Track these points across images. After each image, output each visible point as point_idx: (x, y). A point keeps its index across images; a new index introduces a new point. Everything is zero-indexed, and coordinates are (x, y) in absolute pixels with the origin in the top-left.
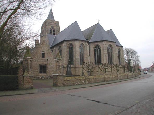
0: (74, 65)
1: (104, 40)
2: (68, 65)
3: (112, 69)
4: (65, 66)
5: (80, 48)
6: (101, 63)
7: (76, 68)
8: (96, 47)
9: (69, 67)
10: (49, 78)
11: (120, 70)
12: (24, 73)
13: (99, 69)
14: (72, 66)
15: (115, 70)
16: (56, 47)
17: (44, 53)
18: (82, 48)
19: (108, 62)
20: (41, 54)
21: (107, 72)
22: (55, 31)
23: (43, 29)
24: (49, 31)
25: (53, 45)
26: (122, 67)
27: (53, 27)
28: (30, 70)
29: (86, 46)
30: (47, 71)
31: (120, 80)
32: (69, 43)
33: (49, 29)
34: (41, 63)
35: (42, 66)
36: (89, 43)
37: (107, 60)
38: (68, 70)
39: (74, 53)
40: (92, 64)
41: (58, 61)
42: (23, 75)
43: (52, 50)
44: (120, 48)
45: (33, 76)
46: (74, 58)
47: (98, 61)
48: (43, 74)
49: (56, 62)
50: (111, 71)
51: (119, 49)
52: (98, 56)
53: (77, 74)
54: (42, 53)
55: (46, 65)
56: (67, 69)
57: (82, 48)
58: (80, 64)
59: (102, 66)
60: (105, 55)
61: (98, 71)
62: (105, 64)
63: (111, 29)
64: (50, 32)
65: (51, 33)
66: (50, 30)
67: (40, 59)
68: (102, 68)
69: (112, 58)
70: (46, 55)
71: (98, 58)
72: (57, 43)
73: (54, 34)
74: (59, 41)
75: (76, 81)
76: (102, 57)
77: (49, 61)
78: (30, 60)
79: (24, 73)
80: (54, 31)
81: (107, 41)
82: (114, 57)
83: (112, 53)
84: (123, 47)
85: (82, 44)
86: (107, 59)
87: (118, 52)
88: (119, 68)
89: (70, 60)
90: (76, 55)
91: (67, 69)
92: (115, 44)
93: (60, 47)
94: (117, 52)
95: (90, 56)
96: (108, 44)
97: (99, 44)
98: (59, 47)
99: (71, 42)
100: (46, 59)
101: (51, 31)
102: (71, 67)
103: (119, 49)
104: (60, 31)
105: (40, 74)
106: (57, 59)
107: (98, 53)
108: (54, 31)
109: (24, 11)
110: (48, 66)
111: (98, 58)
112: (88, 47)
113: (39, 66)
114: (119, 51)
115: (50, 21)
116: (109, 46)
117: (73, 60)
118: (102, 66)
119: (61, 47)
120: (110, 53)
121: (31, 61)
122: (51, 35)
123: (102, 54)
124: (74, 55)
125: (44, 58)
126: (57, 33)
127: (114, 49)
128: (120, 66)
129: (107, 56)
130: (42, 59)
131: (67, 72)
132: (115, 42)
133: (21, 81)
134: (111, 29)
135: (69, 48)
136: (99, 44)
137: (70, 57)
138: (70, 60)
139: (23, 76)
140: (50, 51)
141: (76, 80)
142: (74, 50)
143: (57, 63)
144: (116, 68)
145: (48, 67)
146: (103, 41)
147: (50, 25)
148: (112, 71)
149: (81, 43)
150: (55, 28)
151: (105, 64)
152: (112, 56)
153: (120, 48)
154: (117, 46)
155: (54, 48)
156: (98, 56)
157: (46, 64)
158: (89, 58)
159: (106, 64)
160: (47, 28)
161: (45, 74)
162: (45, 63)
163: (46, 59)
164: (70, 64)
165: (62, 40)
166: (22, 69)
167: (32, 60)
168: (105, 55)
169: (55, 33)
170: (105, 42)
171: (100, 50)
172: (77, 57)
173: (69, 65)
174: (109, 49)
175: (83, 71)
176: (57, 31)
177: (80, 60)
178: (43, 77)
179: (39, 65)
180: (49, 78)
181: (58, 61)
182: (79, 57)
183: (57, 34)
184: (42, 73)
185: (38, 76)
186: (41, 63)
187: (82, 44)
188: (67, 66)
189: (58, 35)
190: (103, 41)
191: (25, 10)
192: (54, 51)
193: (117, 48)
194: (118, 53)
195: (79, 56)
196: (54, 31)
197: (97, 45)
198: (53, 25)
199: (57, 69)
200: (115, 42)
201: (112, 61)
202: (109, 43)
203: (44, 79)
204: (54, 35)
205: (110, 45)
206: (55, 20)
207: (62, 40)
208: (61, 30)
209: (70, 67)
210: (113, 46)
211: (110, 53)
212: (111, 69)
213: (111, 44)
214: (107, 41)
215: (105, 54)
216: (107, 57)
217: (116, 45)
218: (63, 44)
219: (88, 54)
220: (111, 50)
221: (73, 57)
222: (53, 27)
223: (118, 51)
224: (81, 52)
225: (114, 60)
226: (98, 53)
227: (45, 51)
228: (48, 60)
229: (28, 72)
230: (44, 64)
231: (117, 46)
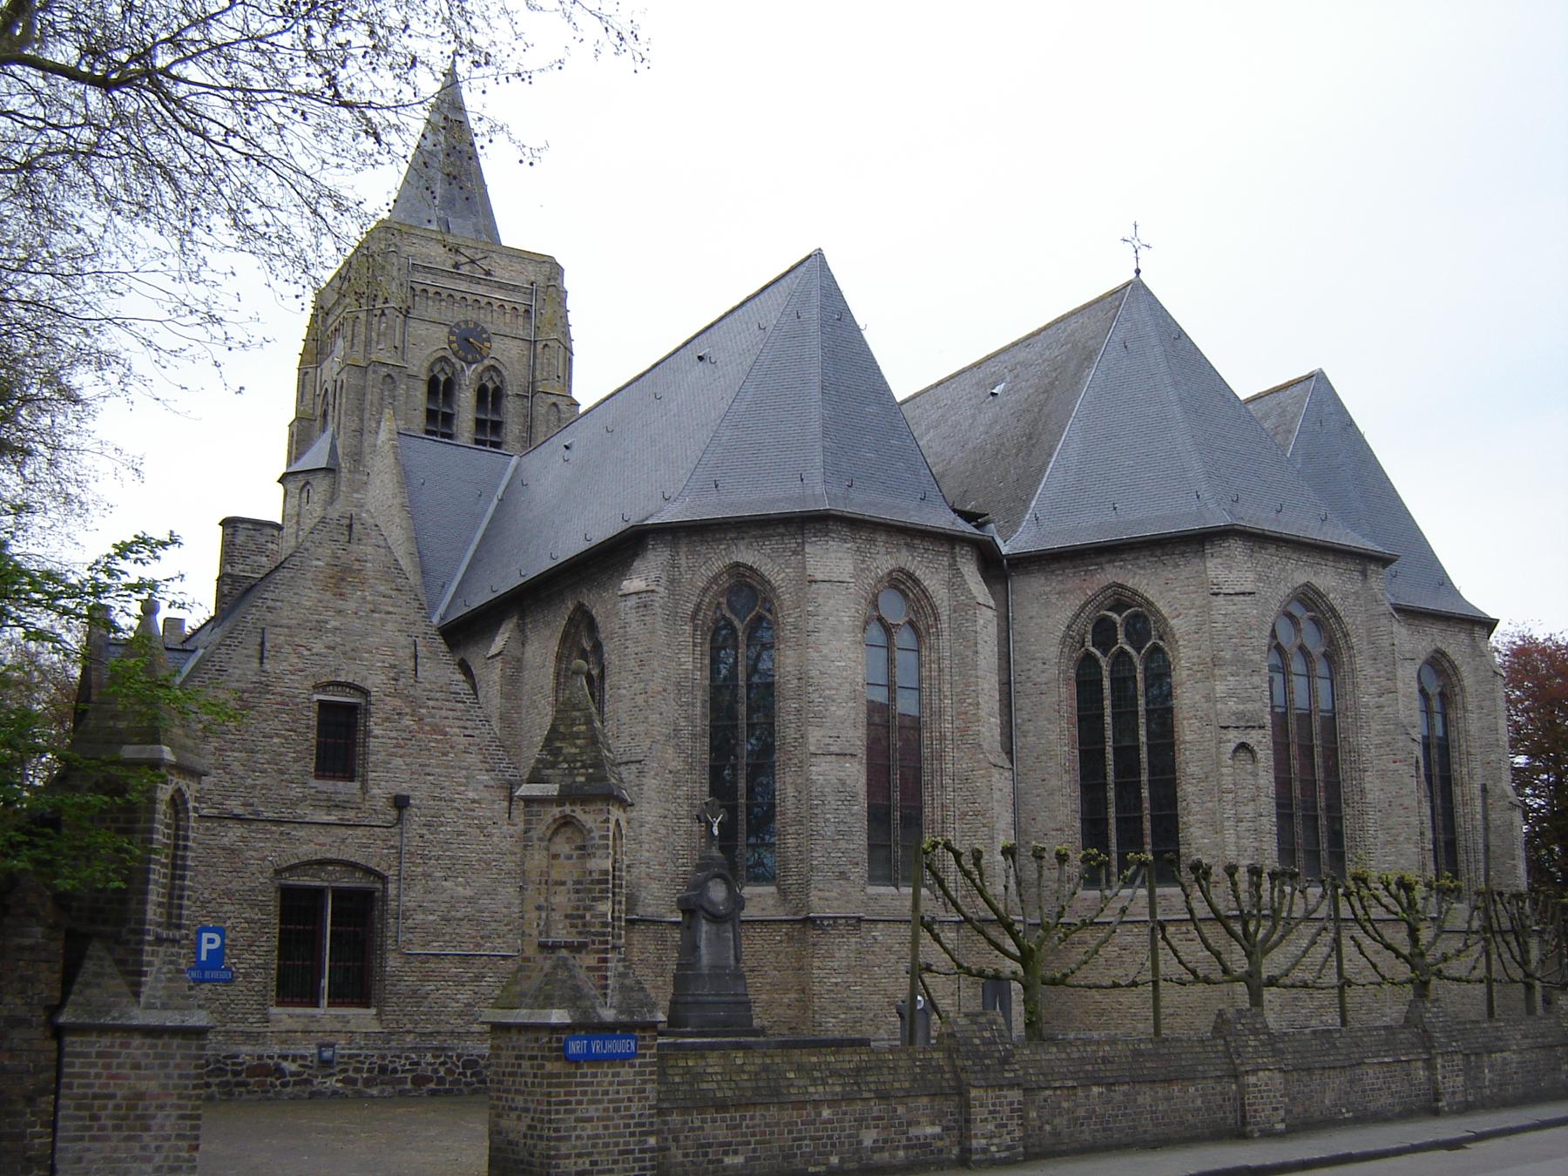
0: (783, 893)
1: (1220, 519)
2: (700, 887)
3: (1348, 948)
4: (658, 900)
5: (875, 632)
6: (1166, 866)
7: (812, 936)
8: (1104, 632)
9: (715, 918)
10: (419, 1081)
11: (1457, 968)
12: (66, 993)
13: (1165, 955)
14: (760, 900)
15: (1385, 960)
16: (521, 628)
17: (352, 708)
18: (904, 638)
19: (1286, 850)
20: (312, 717)
21: (1268, 994)
22: (498, 394)
23: (331, 369)
24: (420, 393)
25: (480, 597)
26: (1487, 928)
27: (469, 342)
28: (159, 941)
29: (964, 608)
30: (393, 962)
31: (1466, 1108)
32: (714, 561)
33: (419, 363)
34: (309, 845)
35: (319, 892)
36: (996, 568)
37: (1269, 823)
38: (705, 957)
39: (787, 709)
40: (1030, 868)
41: (566, 822)
42: (56, 1009)
43: (465, 668)
44: (1455, 645)
45: (200, 1033)
46: (787, 787)
47: (1131, 838)
48: (324, 1012)
49: (540, 829)
50: (1331, 978)
51: (1438, 664)
52: (1127, 755)
53: (833, 1027)
54: (321, 703)
55: (383, 879)
56: (690, 949)
57: (904, 638)
58: (873, 879)
59: (1202, 910)
60: (1243, 746)
61: (1149, 976)
62: (1242, 876)
63: (1317, 381)
64: (431, 415)
65: (439, 422)
66: (433, 384)
67: (296, 791)
68: (1207, 930)
69: (1334, 787)
70: (379, 733)
71: (1128, 788)
72: (546, 564)
73: (489, 432)
74: (570, 544)
75: (826, 1113)
76: (1192, 769)
77: (415, 820)
78: (164, 793)
79: (68, 981)
80: (490, 397)
81: (1258, 539)
82: (1372, 783)
83: (1330, 723)
84: (1490, 625)
85: (901, 582)
86: (1268, 805)
87: (1417, 704)
88: (1453, 944)
89: (732, 811)
90: (815, 736)
91: (690, 949)
92: (1378, 580)
93: (584, 622)
94: (1408, 708)
95: (1009, 752)
96: (1284, 590)
97: (1145, 581)
98: (561, 623)
99: (746, 554)
100: (380, 791)
101: (440, 389)
102: (749, 912)
103: (1438, 664)
104: (577, 393)
105: (285, 1017)
106: (552, 789)
107: (1125, 714)
108: (490, 397)
109: (94, 96)
110: (410, 899)
111: (1128, 788)
112: (986, 623)
113: (273, 907)
114: (1433, 690)
115: (438, 255)
116: (1290, 616)
117: (763, 819)
118: (1202, 910)
119: (592, 626)
120: (1306, 718)
121: (177, 801)
122: (434, 450)
123: (1188, 731)
124: (791, 733)
125: (350, 777)
126: (530, 429)
127: (1359, 661)
128: (1460, 914)
129: (1265, 755)
130: (327, 786)
131: (680, 981)
132: (1384, 561)
133: (30, 1100)
134: (1317, 381)
135: (719, 639)
136: (1145, 581)
137: (720, 788)
138: (732, 811)
139: (58, 1033)
140: (439, 671)
141: (832, 1103)
142: (786, 663)
143: (562, 846)
144: (1398, 937)
145: (401, 915)
146: (1198, 541)
147: (431, 310)
148: (1345, 983)
149: (886, 559)
150: (507, 352)
151: (1242, 876)
152: (1344, 767)
153: (1455, 645)
154: (1410, 614)
155: (499, 643)
156: (1127, 755)
157: (368, 871)
158: (1001, 782)
159: (1255, 871)
160: (382, 353)
161: (362, 1019)
162: (352, 846)
163: (380, 791)
164: (732, 874)
165: (620, 527)
166: (38, 931)
167: (191, 789)
168: (1243, 746)
169: (497, 427)
170: (1237, 548)
171: (1160, 672)
172: (824, 772)
173: (717, 892)
174: (1297, 665)
175: (918, 971)
176: (530, 393)
177: (878, 817)
178: (326, 1063)
179: (278, 872)
180: (419, 1081)
181: (566, 822)
182: (856, 773)
183: (529, 442)
184: (317, 1005)
185: (248, 1036)
186: (307, 851)
187: (901, 582)
188: (691, 909)
189: (534, 461)
190: (1198, 541)
191: (105, 85)
192: (491, 677)
193: (1415, 643)
194: (1418, 718)
195: (861, 753)
196: (482, 393)
197: (1121, 599)
198: (471, 314)
199: (561, 933)
200: (1384, 561)
201: (1336, 837)
202: (1300, 573)
203: (333, 1083)
204: (486, 457)
205: (1308, 597)
206: (510, 236)
207: (604, 529)
208: (589, 386)
209: (729, 917)
210: (1353, 616)
211: (1306, 718)
212: (1321, 950)
213: (1329, 580)
214: (1258, 539)
215: (1234, 738)
216: (1267, 780)
217: (1399, 609)
218: (633, 584)
219: (989, 728)
220: (1321, 668)
221: (764, 763)
222: (469, 342)
223: (1422, 691)
224: (880, 696)
225: (1372, 817)
226: (1125, 714)
227: (367, 685)
228: (401, 803)
229: (133, 974)
230: (353, 866)
231: (1410, 614)
